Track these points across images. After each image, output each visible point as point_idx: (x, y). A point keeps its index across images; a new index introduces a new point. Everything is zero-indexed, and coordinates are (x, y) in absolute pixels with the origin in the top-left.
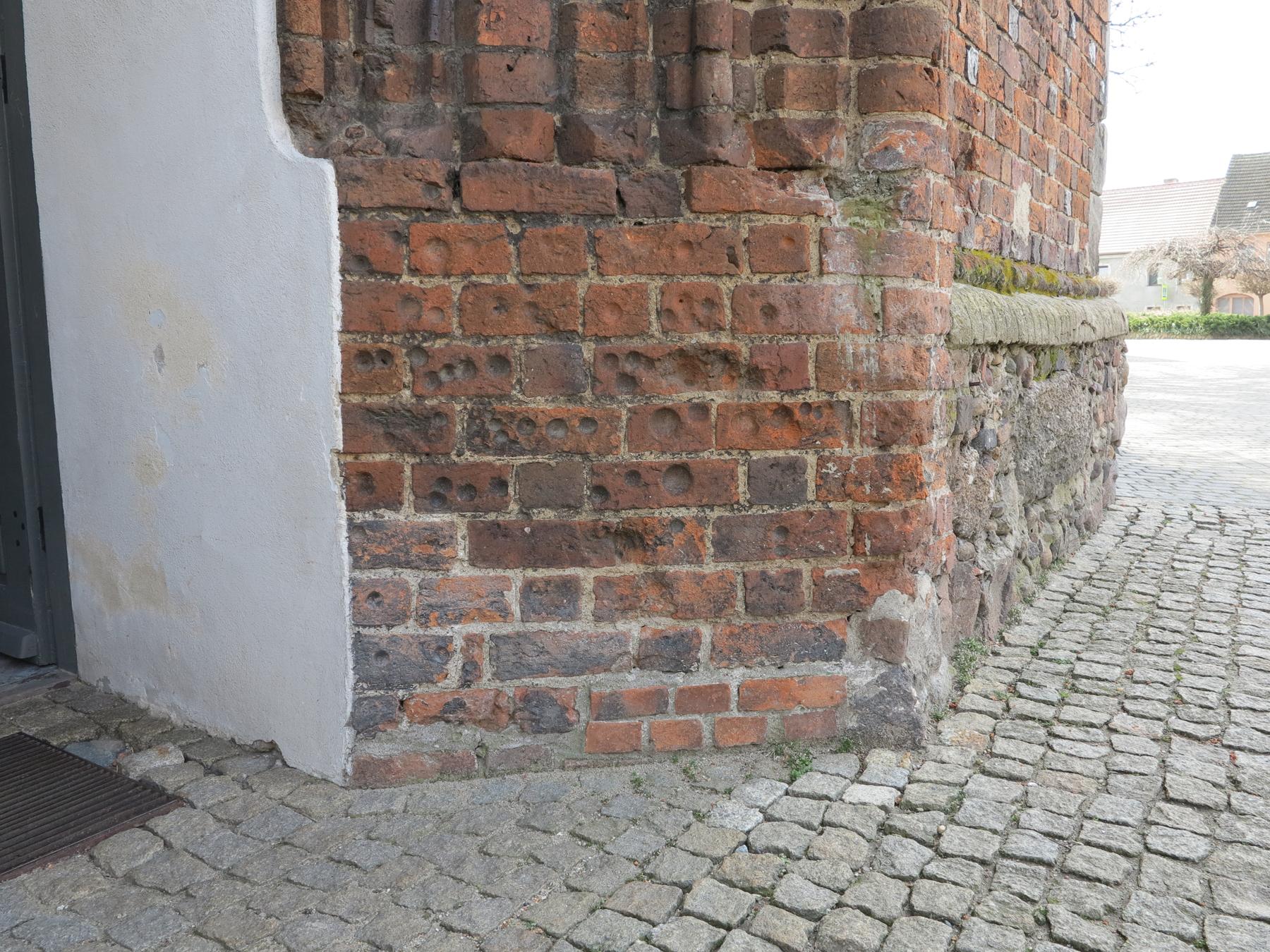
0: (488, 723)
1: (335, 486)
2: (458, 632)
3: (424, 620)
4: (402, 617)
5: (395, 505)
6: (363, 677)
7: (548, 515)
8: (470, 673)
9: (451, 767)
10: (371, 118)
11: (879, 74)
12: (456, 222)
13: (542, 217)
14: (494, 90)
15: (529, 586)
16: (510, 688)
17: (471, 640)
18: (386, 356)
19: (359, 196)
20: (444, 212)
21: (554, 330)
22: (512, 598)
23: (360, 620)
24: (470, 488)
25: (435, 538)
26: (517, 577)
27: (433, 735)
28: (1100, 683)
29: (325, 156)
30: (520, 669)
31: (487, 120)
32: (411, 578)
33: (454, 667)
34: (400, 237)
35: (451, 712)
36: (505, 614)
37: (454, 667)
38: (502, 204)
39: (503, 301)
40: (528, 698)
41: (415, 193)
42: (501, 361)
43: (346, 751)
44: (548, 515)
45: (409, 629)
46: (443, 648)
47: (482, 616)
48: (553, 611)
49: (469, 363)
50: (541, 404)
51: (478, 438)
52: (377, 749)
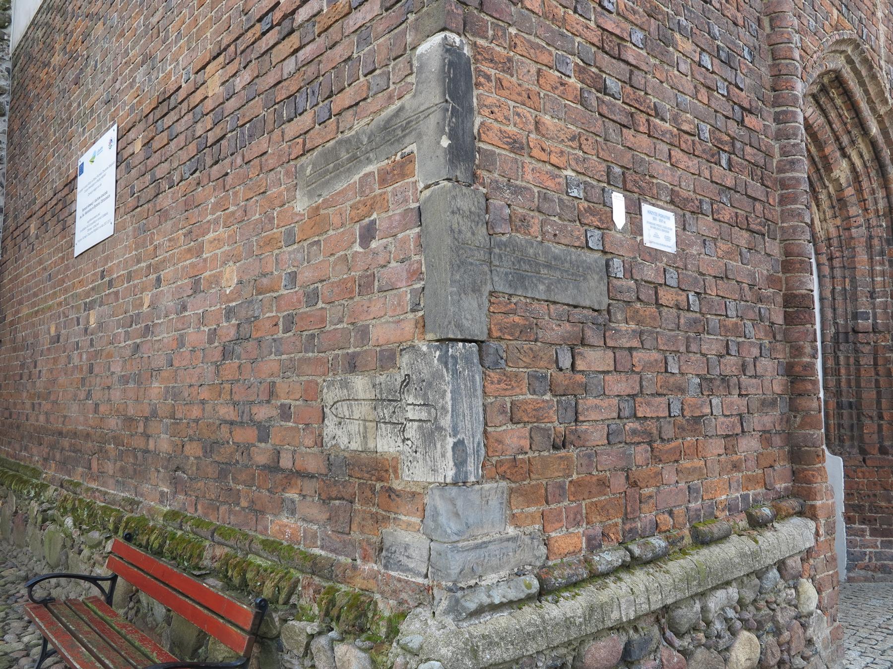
0: (874, 571)
1: (842, 519)
2: (868, 550)
3: (860, 547)
4: (856, 547)
5: (855, 524)
6: (849, 559)
7: (885, 527)
8: (870, 558)
9: (867, 580)
10: (843, 447)
11: (779, 95)
12: (864, 469)
13: (881, 467)
14: (867, 441)
15: (882, 541)
16: (879, 563)
17: (870, 552)
18: (852, 494)
19: (847, 464)
20: (862, 467)
21: (885, 489)
22: (879, 544)
23: (848, 547)
24: (869, 521)
25: (863, 531)
26: (879, 539)
27: (862, 572)
28: (374, 74)
29: (841, 455)
30: (881, 559)
31: (866, 447)
32: (858, 539)
33: (867, 557)
34: (855, 471)
35: (866, 568)
36: (877, 547)
37: (867, 557)
38: (874, 465)
39: (875, 484)
40: (883, 565)
41: (857, 463)
42: (875, 495)
43: (573, 602)
44: (885, 527)
45: (858, 549)
46: (865, 554)
47: (872, 547)
48: (887, 547)
49: (869, 496)
50: (883, 504)
51: (871, 511)
52: (851, 575)
